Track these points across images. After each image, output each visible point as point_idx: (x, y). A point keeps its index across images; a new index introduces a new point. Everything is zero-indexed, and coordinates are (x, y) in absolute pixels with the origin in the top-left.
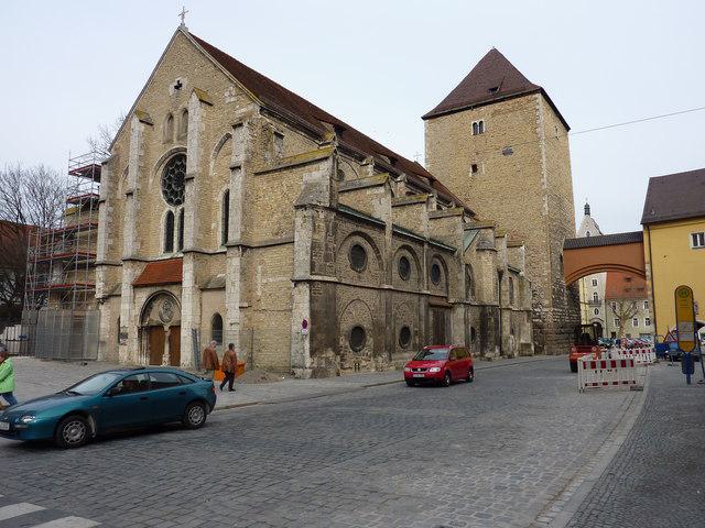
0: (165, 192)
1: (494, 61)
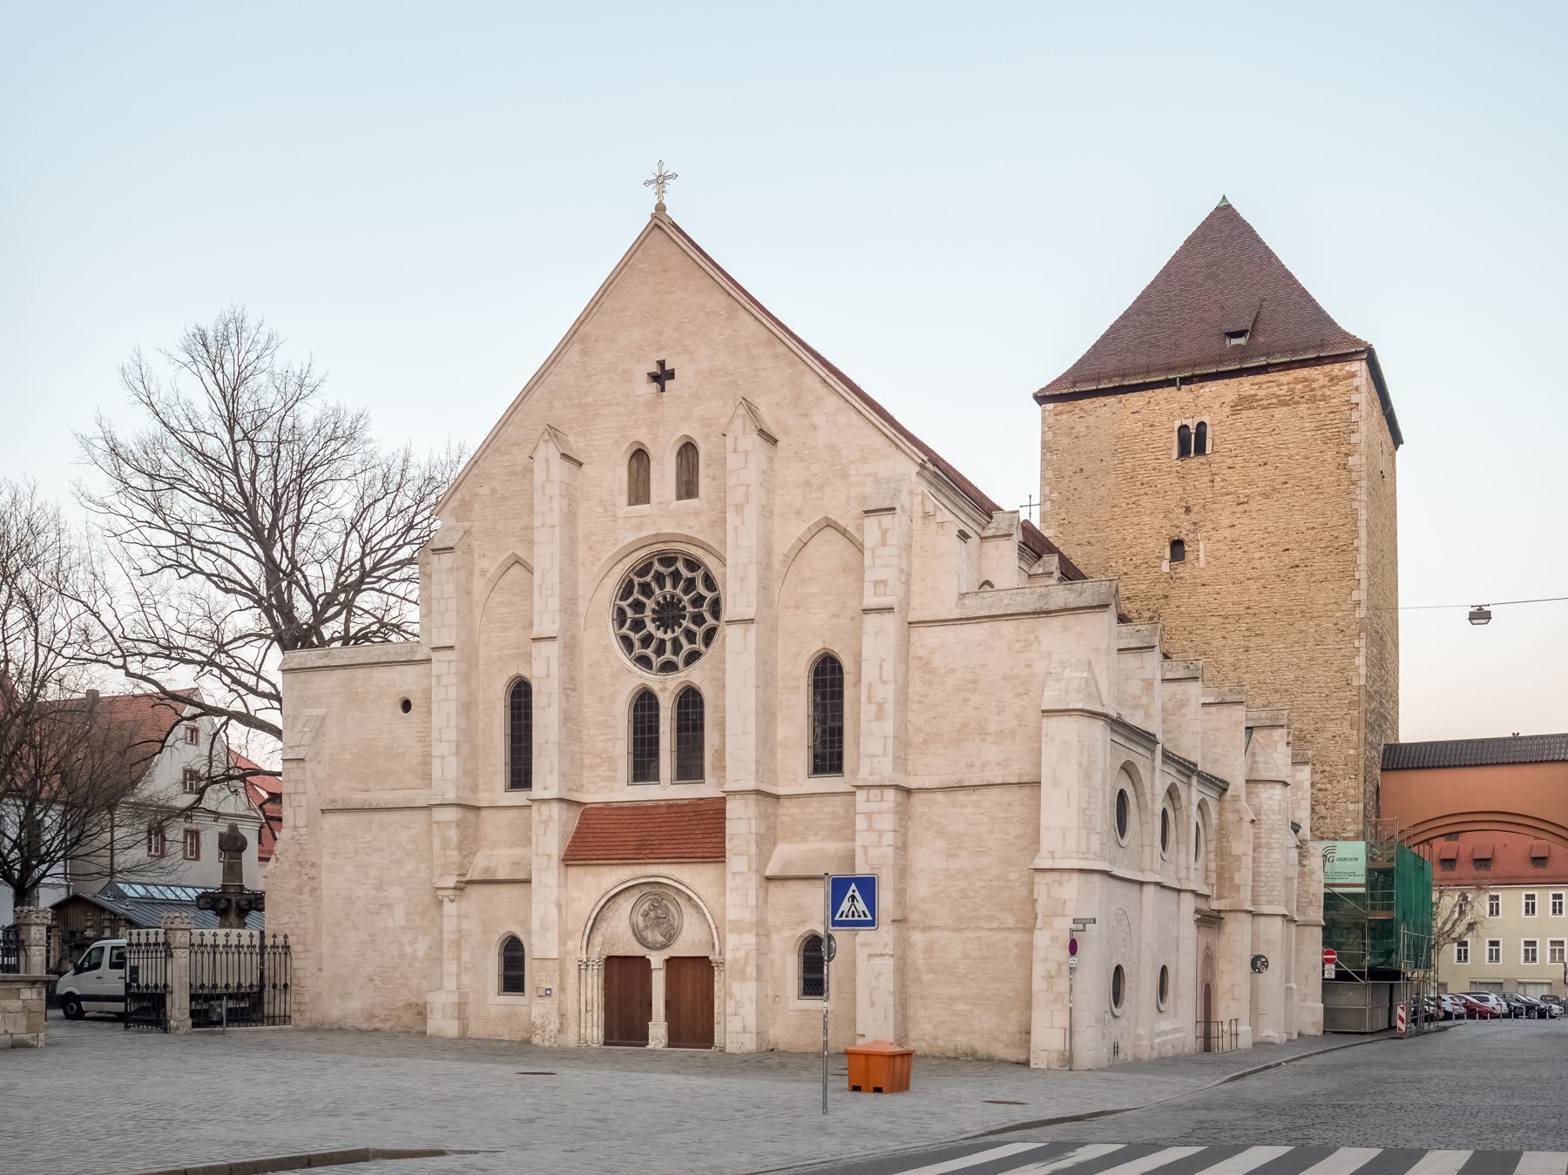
0: (627, 642)
1: (1225, 239)
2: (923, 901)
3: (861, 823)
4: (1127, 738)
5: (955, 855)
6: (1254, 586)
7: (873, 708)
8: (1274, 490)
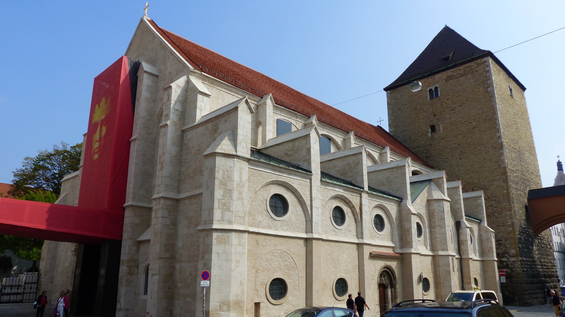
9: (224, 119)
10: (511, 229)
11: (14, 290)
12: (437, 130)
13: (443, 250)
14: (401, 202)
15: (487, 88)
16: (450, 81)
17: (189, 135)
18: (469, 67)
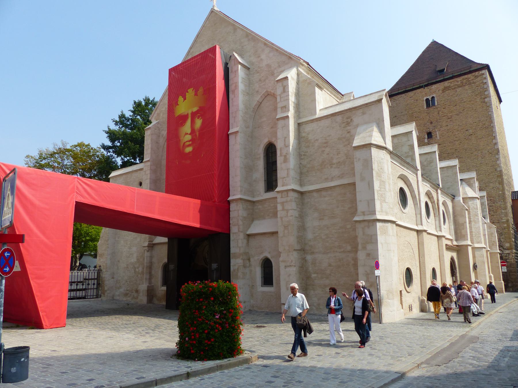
2: (310, 241)
3: (279, 207)
4: (401, 164)
5: (323, 219)
6: (457, 143)
7: (282, 158)
8: (460, 112)
9: (361, 111)
10: (506, 225)
11: (80, 286)
12: (434, 137)
13: (478, 243)
14: (454, 198)
15: (485, 98)
16: (447, 92)
17: (308, 128)
18: (466, 78)
